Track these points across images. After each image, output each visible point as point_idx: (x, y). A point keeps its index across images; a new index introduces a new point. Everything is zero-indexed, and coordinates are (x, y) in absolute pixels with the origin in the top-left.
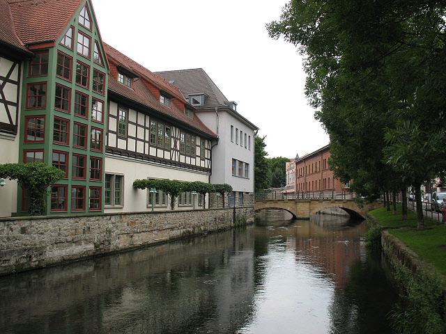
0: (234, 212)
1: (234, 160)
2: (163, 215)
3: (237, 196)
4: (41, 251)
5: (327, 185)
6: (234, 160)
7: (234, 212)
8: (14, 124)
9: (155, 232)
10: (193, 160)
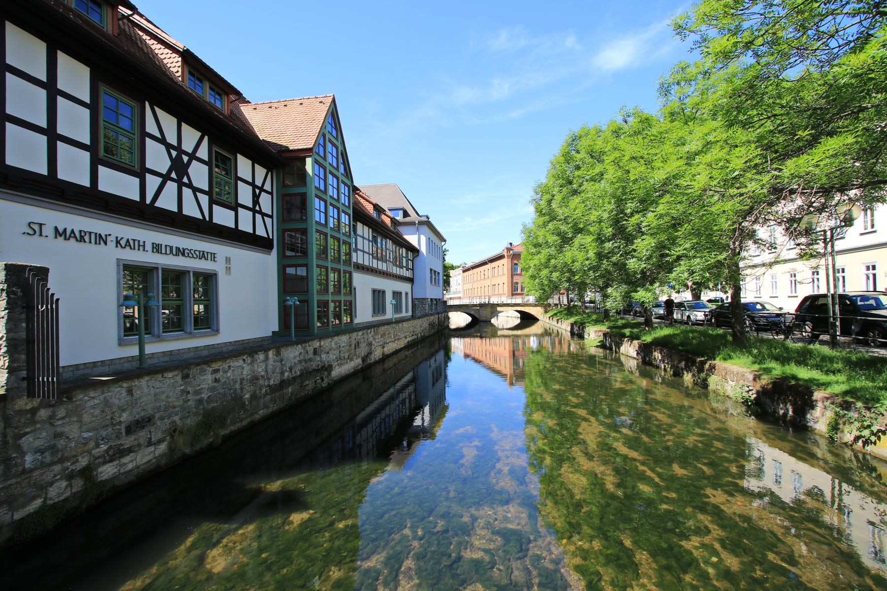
1: (431, 270)
4: (329, 368)
6: (431, 270)
8: (271, 237)
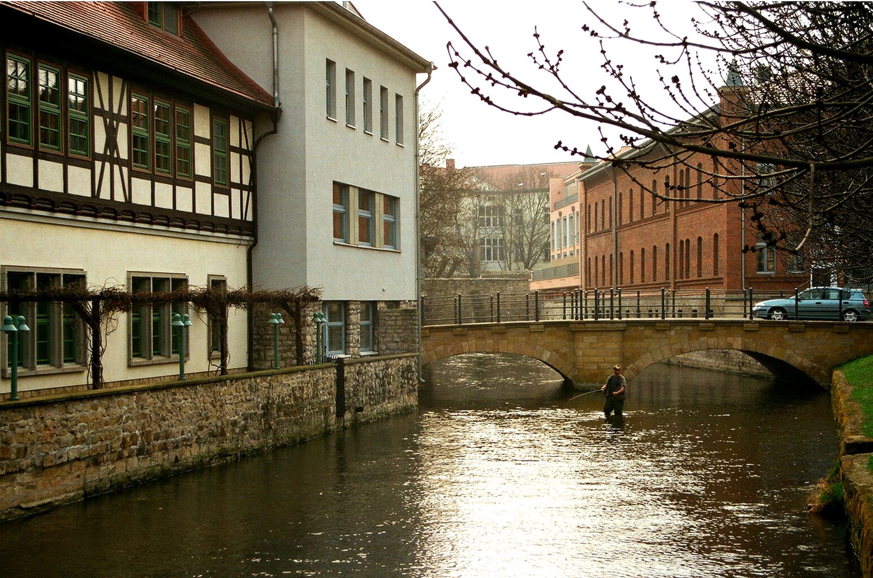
0: (340, 380)
1: (341, 190)
2: (54, 415)
3: (355, 318)
5: (693, 263)
6: (341, 190)
7: (340, 380)
9: (26, 478)
10: (184, 193)
